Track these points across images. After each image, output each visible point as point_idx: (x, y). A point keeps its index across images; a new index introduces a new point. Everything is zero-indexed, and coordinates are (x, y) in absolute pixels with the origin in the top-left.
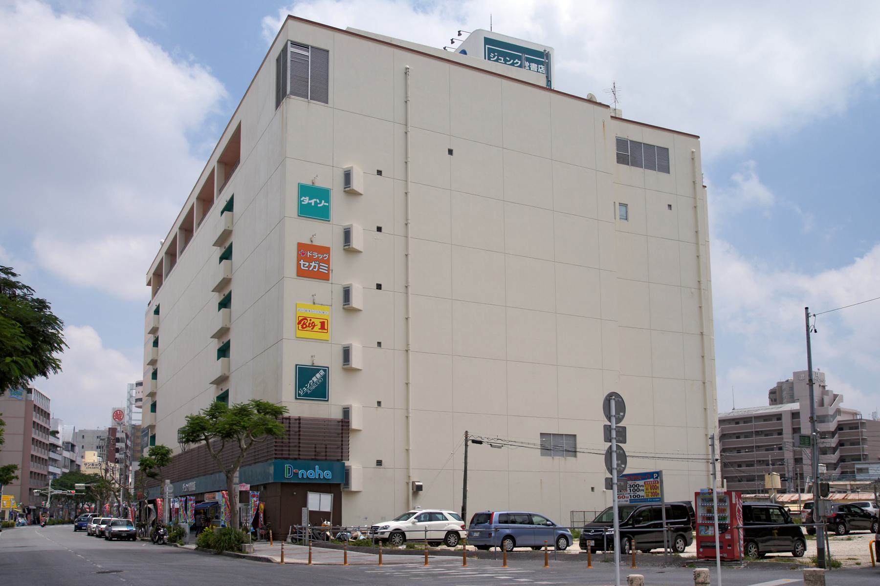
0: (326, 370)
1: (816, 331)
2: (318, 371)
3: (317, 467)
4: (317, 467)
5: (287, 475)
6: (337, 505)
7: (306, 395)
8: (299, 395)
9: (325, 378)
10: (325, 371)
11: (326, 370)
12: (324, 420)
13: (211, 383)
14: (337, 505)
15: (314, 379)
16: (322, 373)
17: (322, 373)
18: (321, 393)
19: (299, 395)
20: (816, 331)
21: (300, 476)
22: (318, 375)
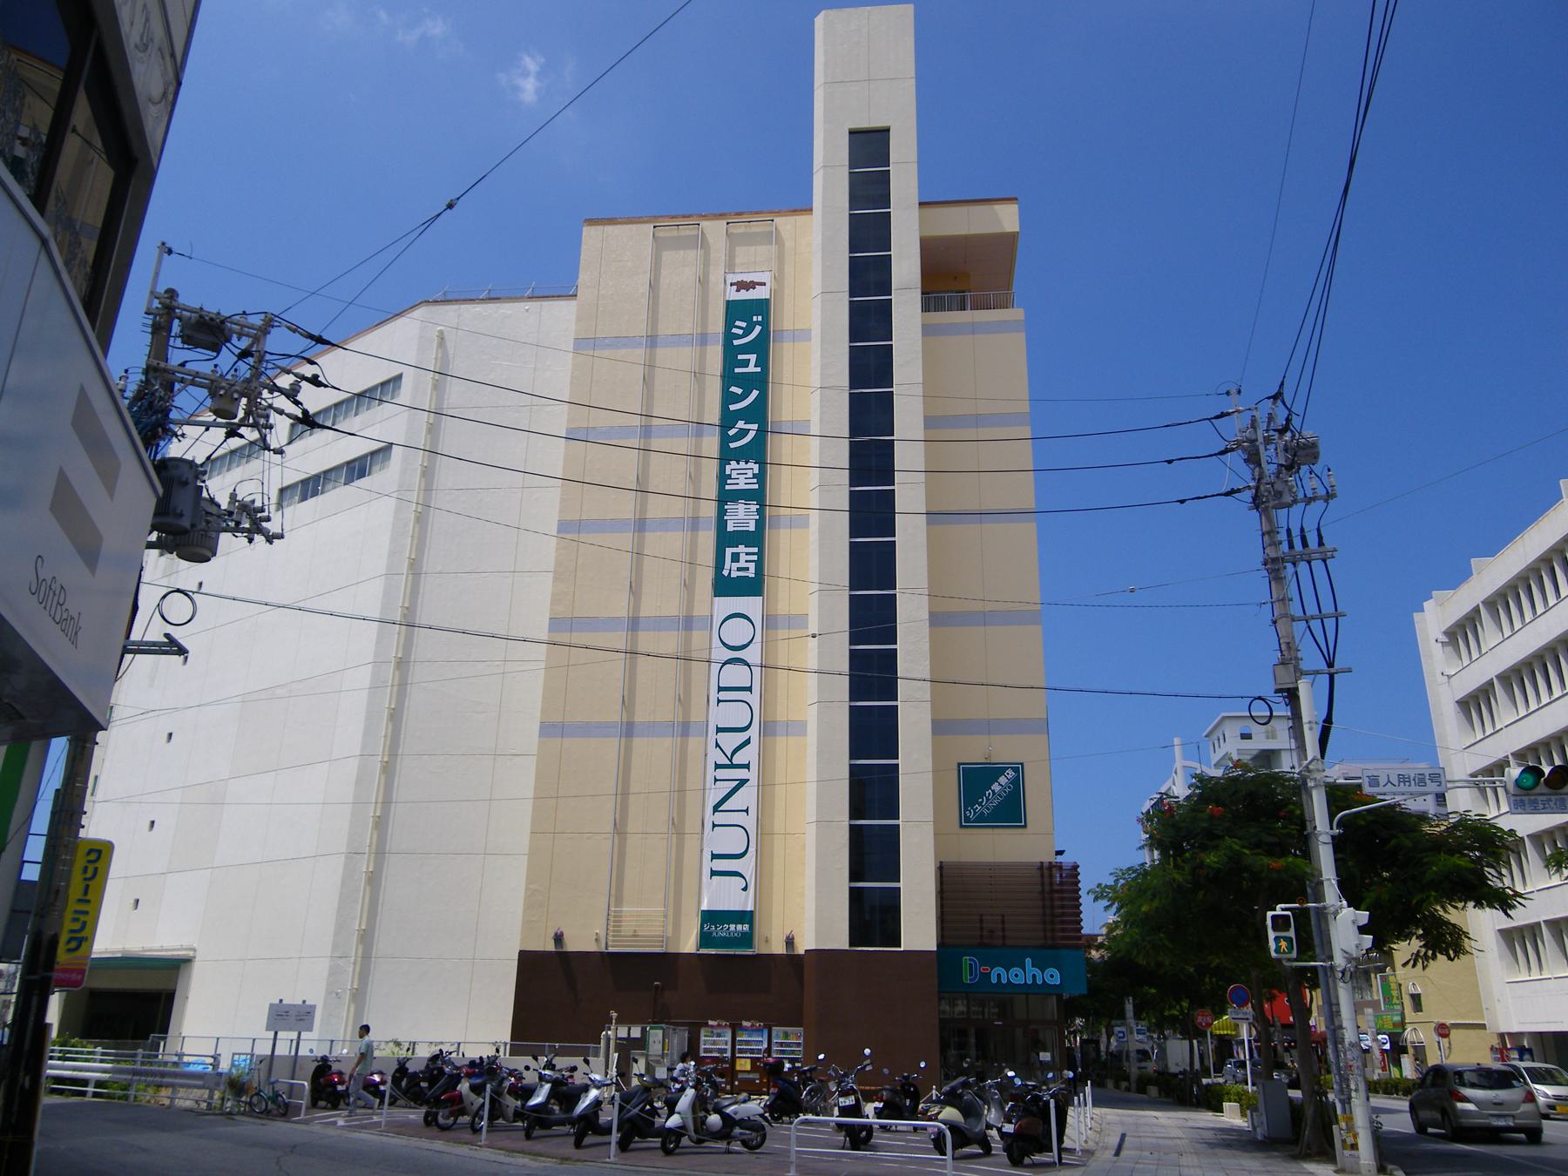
0: (1018, 769)
1: (1060, 853)
2: (1002, 771)
3: (1028, 961)
4: (1028, 961)
5: (967, 979)
6: (761, 477)
7: (981, 818)
8: (967, 819)
9: (1017, 787)
10: (1016, 770)
11: (1018, 769)
12: (991, 867)
13: (93, 572)
14: (761, 477)
15: (996, 787)
16: (1011, 774)
17: (1011, 774)
18: (1010, 811)
19: (967, 819)
20: (1060, 853)
21: (994, 980)
22: (1003, 780)
